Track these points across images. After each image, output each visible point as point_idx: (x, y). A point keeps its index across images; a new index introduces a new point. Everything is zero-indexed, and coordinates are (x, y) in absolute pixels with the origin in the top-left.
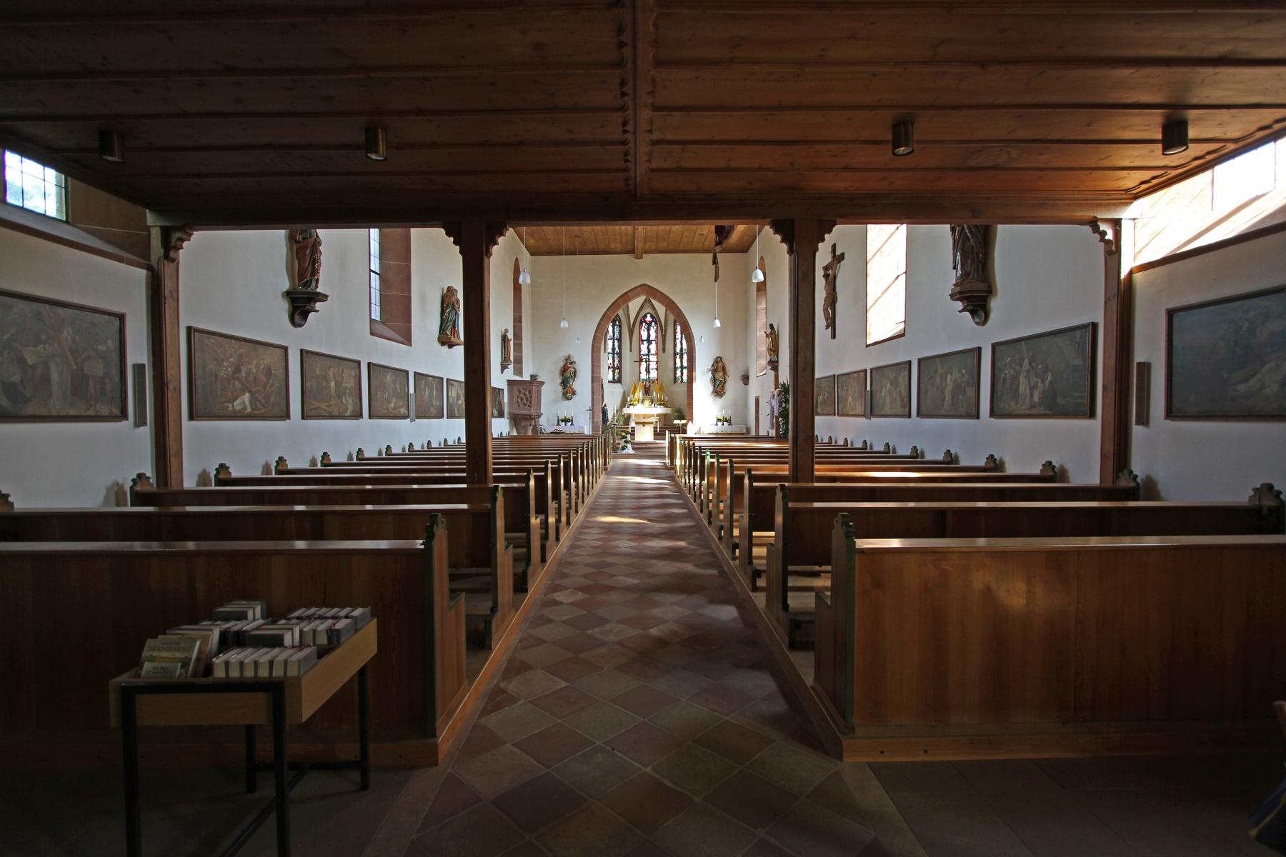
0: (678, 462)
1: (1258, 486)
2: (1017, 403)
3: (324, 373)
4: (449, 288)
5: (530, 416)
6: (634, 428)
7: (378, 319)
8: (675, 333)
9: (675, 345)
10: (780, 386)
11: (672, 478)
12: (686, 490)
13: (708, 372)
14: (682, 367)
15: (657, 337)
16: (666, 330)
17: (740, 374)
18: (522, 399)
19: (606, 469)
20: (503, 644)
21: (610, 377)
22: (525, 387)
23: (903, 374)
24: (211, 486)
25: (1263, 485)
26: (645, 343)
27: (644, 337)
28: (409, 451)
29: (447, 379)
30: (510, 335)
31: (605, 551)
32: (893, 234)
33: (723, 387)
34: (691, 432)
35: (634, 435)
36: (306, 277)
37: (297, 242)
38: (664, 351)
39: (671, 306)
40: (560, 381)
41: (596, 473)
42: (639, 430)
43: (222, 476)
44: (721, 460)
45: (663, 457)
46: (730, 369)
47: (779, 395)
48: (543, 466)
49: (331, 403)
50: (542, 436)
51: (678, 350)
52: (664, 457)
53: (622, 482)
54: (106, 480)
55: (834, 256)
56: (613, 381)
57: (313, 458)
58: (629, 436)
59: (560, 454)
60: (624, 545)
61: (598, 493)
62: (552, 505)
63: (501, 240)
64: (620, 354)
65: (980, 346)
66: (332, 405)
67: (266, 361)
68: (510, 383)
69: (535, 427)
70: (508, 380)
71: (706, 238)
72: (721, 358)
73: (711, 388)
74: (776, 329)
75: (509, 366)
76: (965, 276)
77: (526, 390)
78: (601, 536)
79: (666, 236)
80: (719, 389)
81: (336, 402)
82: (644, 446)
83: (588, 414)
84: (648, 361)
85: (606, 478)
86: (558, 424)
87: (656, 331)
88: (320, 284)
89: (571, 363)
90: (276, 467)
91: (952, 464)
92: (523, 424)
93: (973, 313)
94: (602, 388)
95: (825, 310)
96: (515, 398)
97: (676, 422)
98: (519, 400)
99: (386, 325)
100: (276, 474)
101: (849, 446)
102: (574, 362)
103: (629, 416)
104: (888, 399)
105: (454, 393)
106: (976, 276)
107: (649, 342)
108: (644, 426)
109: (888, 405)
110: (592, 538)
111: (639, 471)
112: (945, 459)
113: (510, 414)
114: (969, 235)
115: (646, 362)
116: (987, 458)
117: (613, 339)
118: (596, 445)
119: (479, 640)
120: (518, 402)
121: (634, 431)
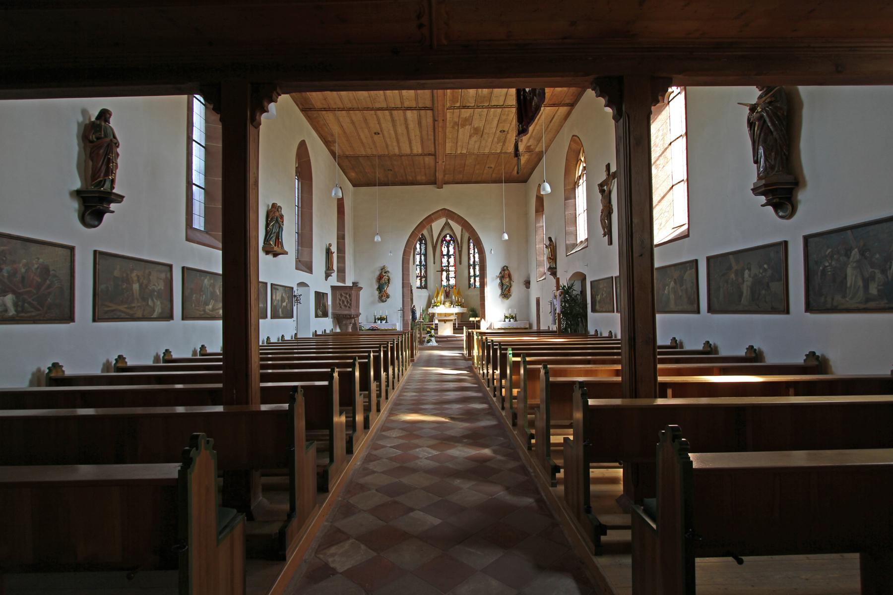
0: (475, 352)
1: (748, 347)
2: (844, 297)
3: (125, 275)
4: (274, 205)
5: (350, 315)
6: (437, 324)
7: (202, 229)
8: (469, 249)
10: (561, 288)
11: (470, 369)
12: (481, 376)
13: (497, 278)
14: (475, 276)
15: (454, 253)
17: (522, 279)
18: (343, 302)
19: (413, 361)
21: (418, 283)
22: (346, 292)
23: (688, 272)
24: (197, 356)
25: (810, 352)
27: (445, 252)
28: (295, 338)
29: (272, 284)
30: (334, 249)
31: (403, 467)
32: (666, 149)
33: (509, 290)
34: (484, 327)
35: (437, 330)
36: (99, 177)
37: (92, 142)
38: (460, 263)
39: (466, 226)
40: (377, 287)
41: (403, 365)
42: (441, 325)
43: (119, 365)
44: (528, 359)
45: (461, 348)
46: (515, 276)
47: (560, 295)
48: (367, 354)
49: (133, 305)
50: (361, 333)
51: (472, 262)
52: (462, 348)
53: (427, 374)
54: (31, 368)
55: (609, 174)
56: (421, 287)
57: (195, 349)
58: (433, 331)
59: (380, 344)
60: (425, 455)
61: (404, 385)
62: (359, 399)
63: (272, 106)
64: (426, 266)
65: (696, 258)
66: (134, 307)
67: (41, 260)
68: (334, 288)
69: (355, 325)
70: (331, 286)
71: (493, 171)
73: (499, 291)
74: (554, 242)
75: (332, 274)
76: (769, 168)
77: (347, 294)
78: (412, 407)
79: (461, 169)
80: (506, 292)
81: (139, 304)
82: (446, 340)
83: (400, 313)
84: (448, 271)
85: (412, 370)
86: (375, 322)
87: (454, 248)
88: (116, 186)
89: (385, 273)
90: (200, 352)
91: (712, 354)
92: (344, 322)
93: (777, 207)
94: (412, 293)
95: (602, 220)
96: (338, 301)
97: (471, 319)
98: (341, 303)
99: (210, 235)
100: (200, 356)
101: (613, 338)
102: (388, 272)
103: (433, 315)
104: (672, 296)
105: (278, 296)
106: (781, 169)
107: (449, 256)
108: (445, 323)
109: (672, 302)
110: (390, 446)
111: (442, 362)
112: (748, 355)
113: (333, 314)
114: (771, 127)
115: (446, 271)
116: (704, 344)
117: (420, 254)
118: (402, 342)
120: (340, 304)
121: (437, 327)
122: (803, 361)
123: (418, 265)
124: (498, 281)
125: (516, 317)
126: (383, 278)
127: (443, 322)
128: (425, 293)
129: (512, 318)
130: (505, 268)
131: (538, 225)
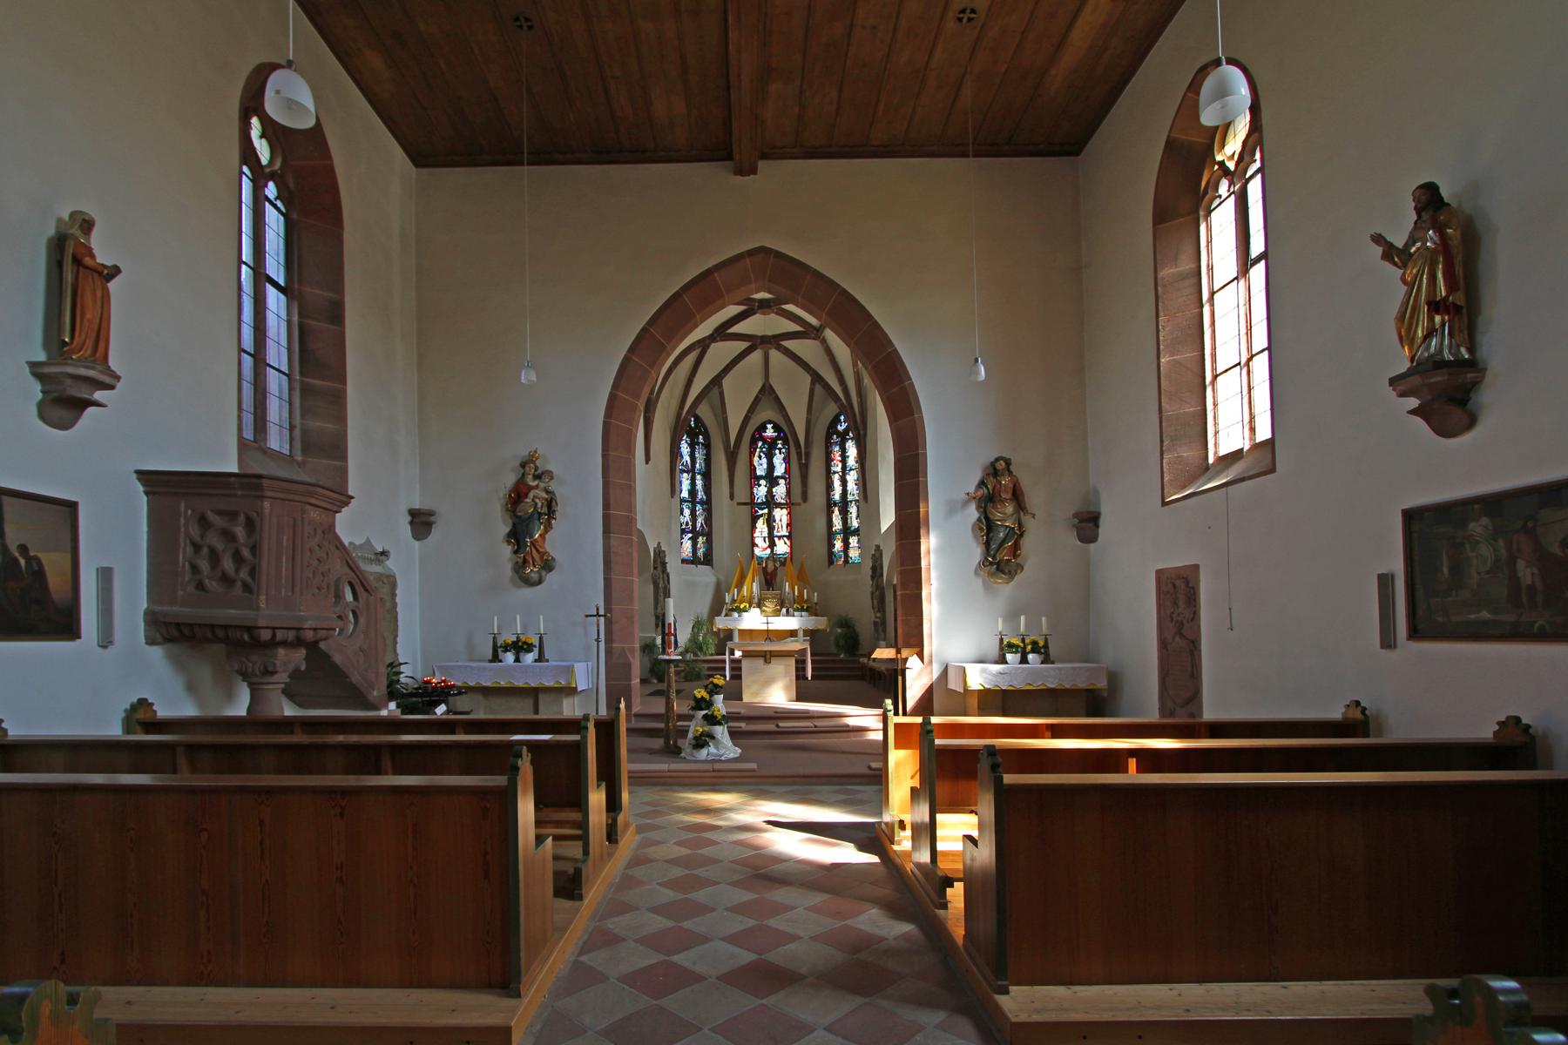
5: (250, 629)
9: (829, 487)
15: (787, 470)
16: (808, 455)
18: (214, 557)
20: (594, 893)
25: (1509, 718)
26: (763, 482)
27: (761, 471)
33: (1016, 546)
38: (805, 497)
40: (507, 530)
46: (1035, 497)
51: (837, 496)
56: (694, 560)
64: (707, 504)
72: (1008, 462)
73: (977, 552)
77: (232, 515)
82: (771, 727)
87: (787, 460)
89: (537, 477)
96: (184, 552)
98: (205, 566)
102: (550, 474)
103: (729, 634)
107: (772, 481)
108: (767, 661)
117: (692, 471)
119: (569, 886)
120: (195, 569)
121: (740, 669)
122: (1491, 735)
123: (686, 501)
124: (973, 513)
125: (1046, 646)
126: (526, 496)
127: (761, 661)
128: (705, 576)
129: (1033, 651)
130: (1001, 465)
131: (1166, 272)
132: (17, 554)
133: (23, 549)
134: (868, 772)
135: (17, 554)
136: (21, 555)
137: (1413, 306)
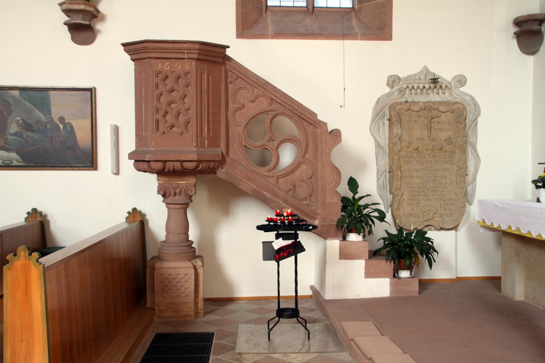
132: (58, 123)
133: (62, 119)
134: (3, 164)
135: (58, 123)
136: (60, 122)
137: (205, 114)
